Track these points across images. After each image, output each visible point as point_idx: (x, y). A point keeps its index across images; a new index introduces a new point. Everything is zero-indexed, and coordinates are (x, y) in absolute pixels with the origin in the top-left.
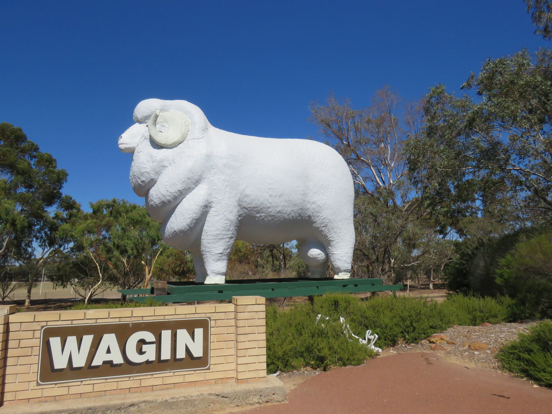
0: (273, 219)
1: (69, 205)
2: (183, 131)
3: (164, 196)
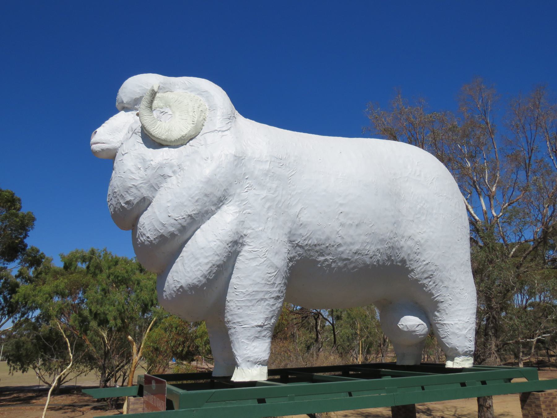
0: (346, 265)
1: (36, 260)
2: (196, 120)
3: (163, 225)
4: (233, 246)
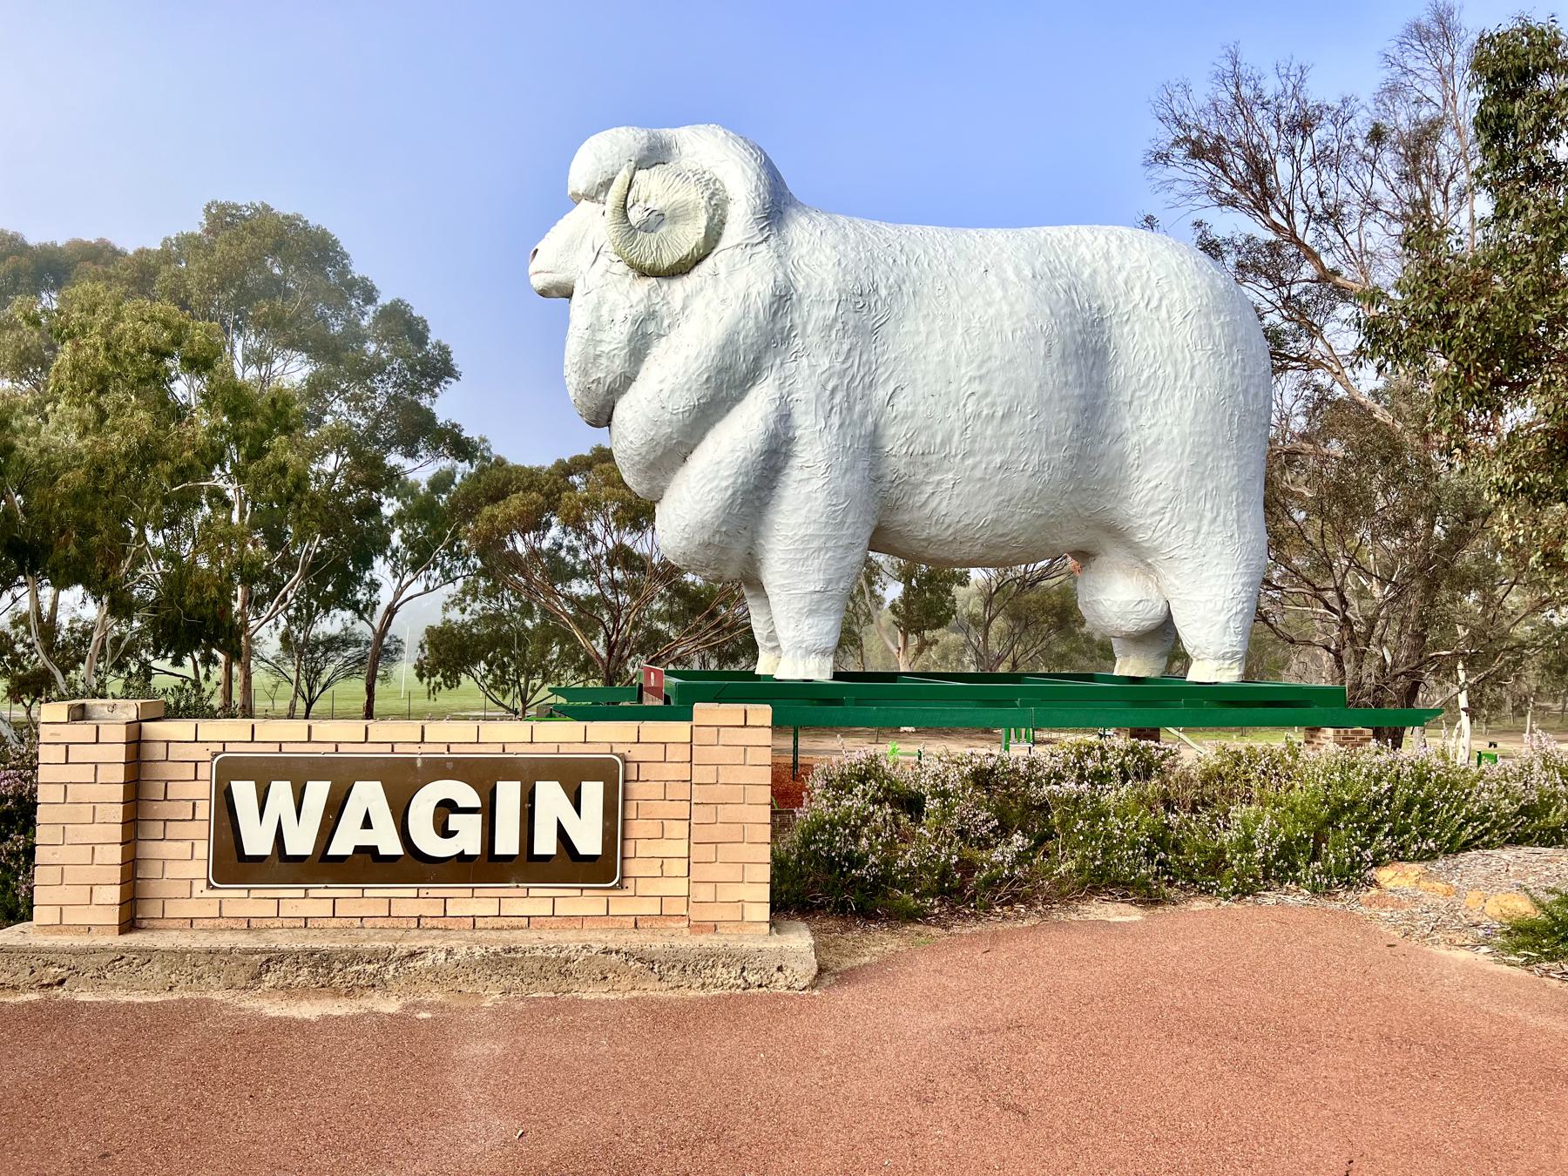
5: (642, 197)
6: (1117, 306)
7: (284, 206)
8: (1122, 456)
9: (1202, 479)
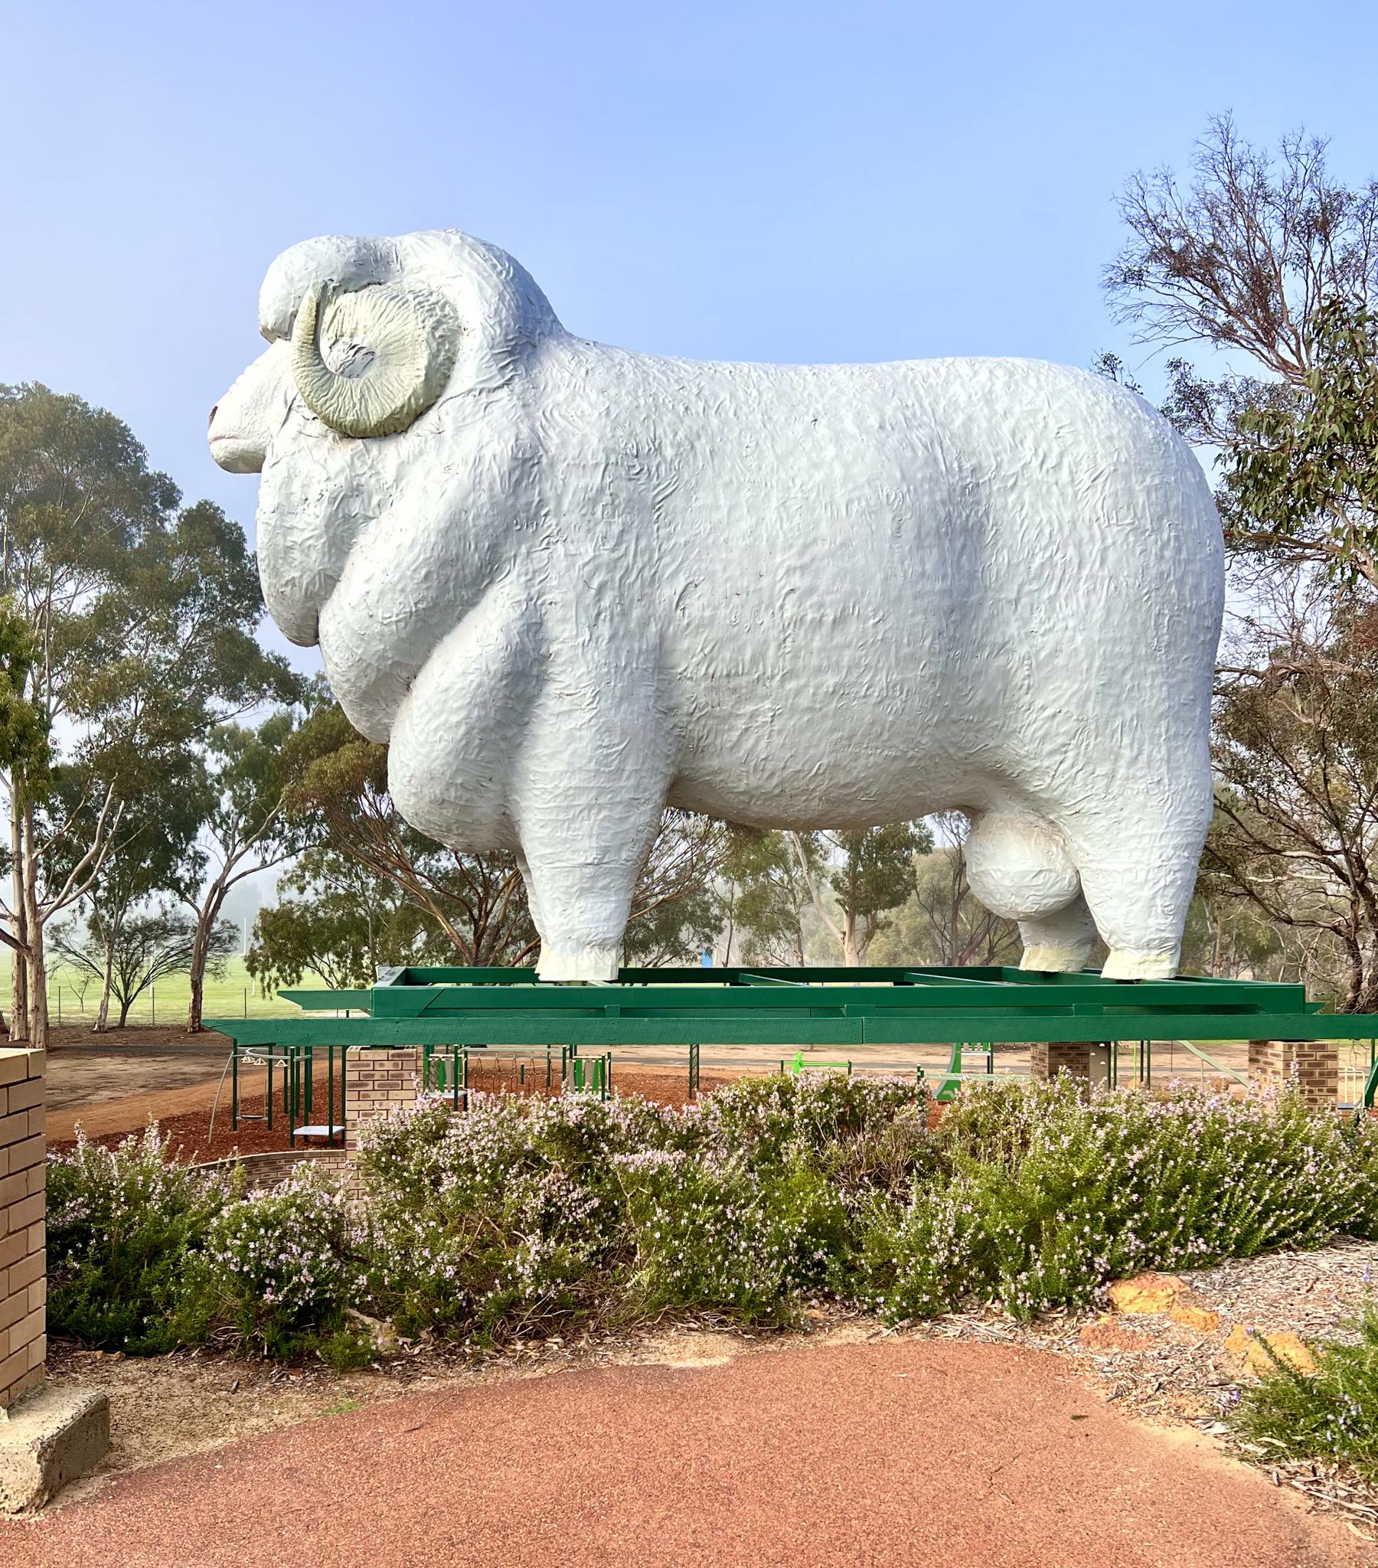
4: (517, 684)
5: (347, 329)
6: (999, 466)
7: (60, 389)
8: (1006, 674)
9: (1117, 704)
